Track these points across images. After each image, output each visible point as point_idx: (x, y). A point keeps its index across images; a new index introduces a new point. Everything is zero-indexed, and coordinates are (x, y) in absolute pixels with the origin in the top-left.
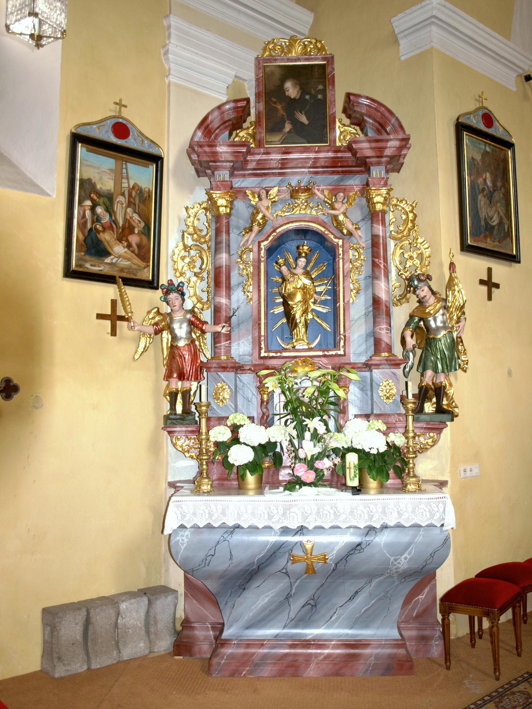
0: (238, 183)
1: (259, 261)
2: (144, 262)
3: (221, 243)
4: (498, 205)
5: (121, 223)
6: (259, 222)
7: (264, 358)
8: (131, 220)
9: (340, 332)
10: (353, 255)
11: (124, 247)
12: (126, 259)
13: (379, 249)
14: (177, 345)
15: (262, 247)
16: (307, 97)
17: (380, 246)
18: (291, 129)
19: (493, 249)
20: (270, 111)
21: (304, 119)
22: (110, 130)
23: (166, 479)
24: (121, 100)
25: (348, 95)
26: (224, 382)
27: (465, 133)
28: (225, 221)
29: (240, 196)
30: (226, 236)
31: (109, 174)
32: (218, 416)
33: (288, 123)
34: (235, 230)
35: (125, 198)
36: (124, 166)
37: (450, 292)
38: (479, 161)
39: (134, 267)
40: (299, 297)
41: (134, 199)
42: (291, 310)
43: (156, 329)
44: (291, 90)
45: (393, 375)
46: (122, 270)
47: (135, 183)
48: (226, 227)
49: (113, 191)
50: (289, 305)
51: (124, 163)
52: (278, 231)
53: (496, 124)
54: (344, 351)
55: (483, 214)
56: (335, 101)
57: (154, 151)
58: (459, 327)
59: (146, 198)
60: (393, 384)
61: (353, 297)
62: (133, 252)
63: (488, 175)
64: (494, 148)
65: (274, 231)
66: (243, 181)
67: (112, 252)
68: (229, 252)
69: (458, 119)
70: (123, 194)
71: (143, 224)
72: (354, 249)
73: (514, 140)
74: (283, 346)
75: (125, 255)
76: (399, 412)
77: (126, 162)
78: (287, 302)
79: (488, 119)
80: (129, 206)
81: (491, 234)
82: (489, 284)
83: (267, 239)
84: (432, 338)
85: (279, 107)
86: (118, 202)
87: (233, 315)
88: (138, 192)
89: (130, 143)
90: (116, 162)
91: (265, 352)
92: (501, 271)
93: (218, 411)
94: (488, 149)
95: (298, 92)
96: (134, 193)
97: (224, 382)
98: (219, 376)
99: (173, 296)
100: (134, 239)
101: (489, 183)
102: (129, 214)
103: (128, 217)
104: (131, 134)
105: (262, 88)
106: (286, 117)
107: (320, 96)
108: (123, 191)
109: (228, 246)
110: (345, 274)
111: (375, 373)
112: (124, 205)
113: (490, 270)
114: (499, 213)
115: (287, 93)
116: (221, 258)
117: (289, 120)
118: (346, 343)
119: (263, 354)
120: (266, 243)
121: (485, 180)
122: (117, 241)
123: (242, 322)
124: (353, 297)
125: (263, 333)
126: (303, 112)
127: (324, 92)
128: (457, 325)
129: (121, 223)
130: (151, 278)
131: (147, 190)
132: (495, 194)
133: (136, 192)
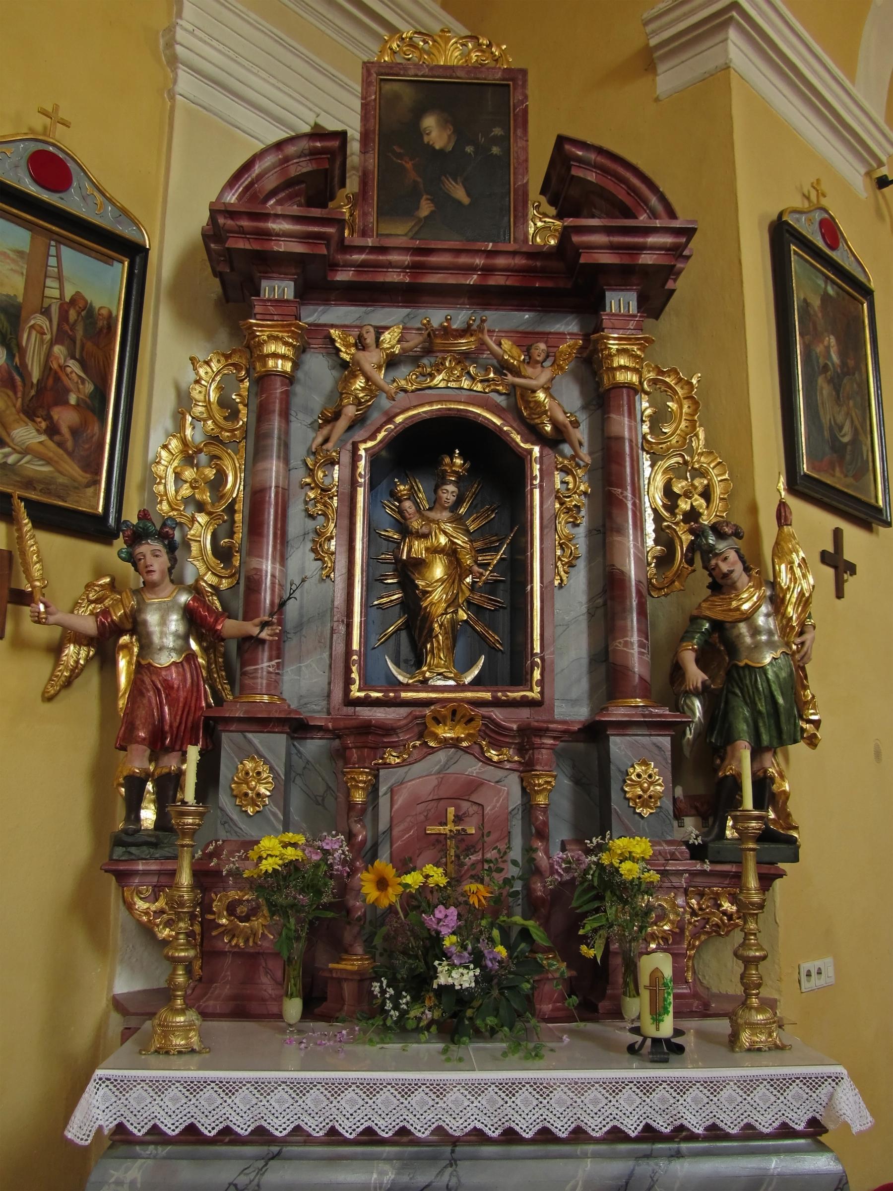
0: (313, 315)
1: (354, 484)
2: (85, 472)
3: (268, 435)
4: (851, 403)
5: (35, 376)
6: (356, 397)
7: (359, 702)
8: (61, 374)
9: (532, 648)
10: (562, 482)
11: (38, 431)
12: (42, 459)
13: (625, 467)
14: (150, 665)
15: (362, 453)
16: (469, 149)
17: (625, 461)
18: (432, 212)
19: (846, 490)
20: (387, 166)
21: (460, 193)
22: (23, 163)
23: (110, 987)
24: (56, 108)
25: (561, 140)
26: (261, 756)
27: (793, 247)
28: (279, 389)
29: (316, 343)
30: (280, 422)
31: (13, 260)
32: (242, 839)
33: (428, 199)
34: (301, 416)
35: (51, 321)
36: (53, 251)
37: (783, 567)
38: (816, 308)
39: (61, 480)
40: (438, 571)
41: (73, 327)
42: (420, 600)
43: (103, 623)
44: (435, 131)
45: (656, 751)
46: (29, 483)
47: (78, 293)
48: (281, 403)
49: (20, 299)
50: (417, 586)
51: (53, 243)
52: (399, 419)
53: (842, 244)
54: (542, 693)
55: (826, 419)
56: (526, 160)
57: (126, 231)
58: (803, 643)
59: (101, 330)
60: (656, 770)
61: (562, 573)
62: (60, 445)
63: (833, 340)
64: (841, 292)
65: (390, 420)
66: (324, 312)
67: (8, 440)
68: (286, 459)
69: (780, 215)
70: (46, 312)
71: (89, 387)
72: (561, 470)
73: (872, 285)
74: (400, 678)
75: (41, 449)
76: (669, 838)
77: (58, 242)
78: (413, 581)
79: (830, 229)
80: (58, 339)
81: (842, 458)
82: (836, 562)
83: (372, 437)
84: (743, 668)
85: (409, 166)
86: (32, 327)
87: (289, 598)
88: (83, 313)
89: (72, 202)
90: (32, 238)
91: (360, 690)
92: (855, 538)
93: (243, 826)
94: (831, 291)
95: (449, 137)
96: (72, 315)
97: (261, 756)
98: (250, 742)
99: (149, 549)
100: (65, 418)
101: (835, 358)
102: (57, 359)
103: (55, 366)
104: (75, 184)
105: (374, 124)
106: (421, 186)
107: (495, 150)
108: (45, 305)
109: (285, 445)
110: (545, 522)
111: (616, 744)
112: (48, 337)
113: (837, 534)
114: (852, 422)
115: (426, 139)
116: (265, 470)
117: (428, 194)
118: (546, 675)
119: (356, 693)
120: (370, 444)
121: (828, 348)
122: (22, 415)
123: (309, 621)
124: (562, 573)
125: (355, 646)
126: (459, 180)
127: (504, 141)
128: (798, 640)
129: (35, 376)
130: (100, 509)
131: (104, 312)
132: (845, 381)
133: (79, 314)
